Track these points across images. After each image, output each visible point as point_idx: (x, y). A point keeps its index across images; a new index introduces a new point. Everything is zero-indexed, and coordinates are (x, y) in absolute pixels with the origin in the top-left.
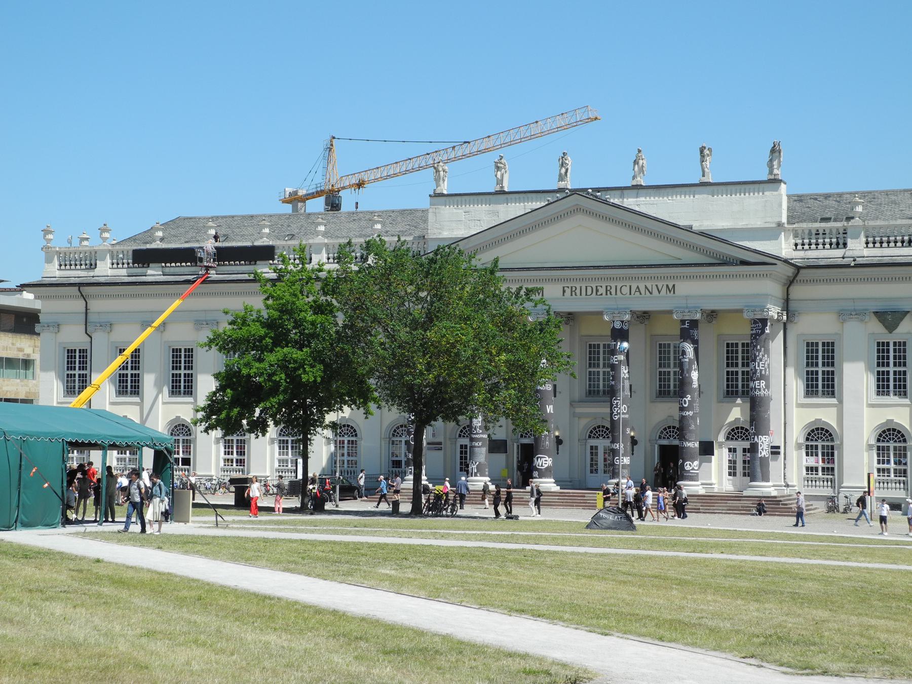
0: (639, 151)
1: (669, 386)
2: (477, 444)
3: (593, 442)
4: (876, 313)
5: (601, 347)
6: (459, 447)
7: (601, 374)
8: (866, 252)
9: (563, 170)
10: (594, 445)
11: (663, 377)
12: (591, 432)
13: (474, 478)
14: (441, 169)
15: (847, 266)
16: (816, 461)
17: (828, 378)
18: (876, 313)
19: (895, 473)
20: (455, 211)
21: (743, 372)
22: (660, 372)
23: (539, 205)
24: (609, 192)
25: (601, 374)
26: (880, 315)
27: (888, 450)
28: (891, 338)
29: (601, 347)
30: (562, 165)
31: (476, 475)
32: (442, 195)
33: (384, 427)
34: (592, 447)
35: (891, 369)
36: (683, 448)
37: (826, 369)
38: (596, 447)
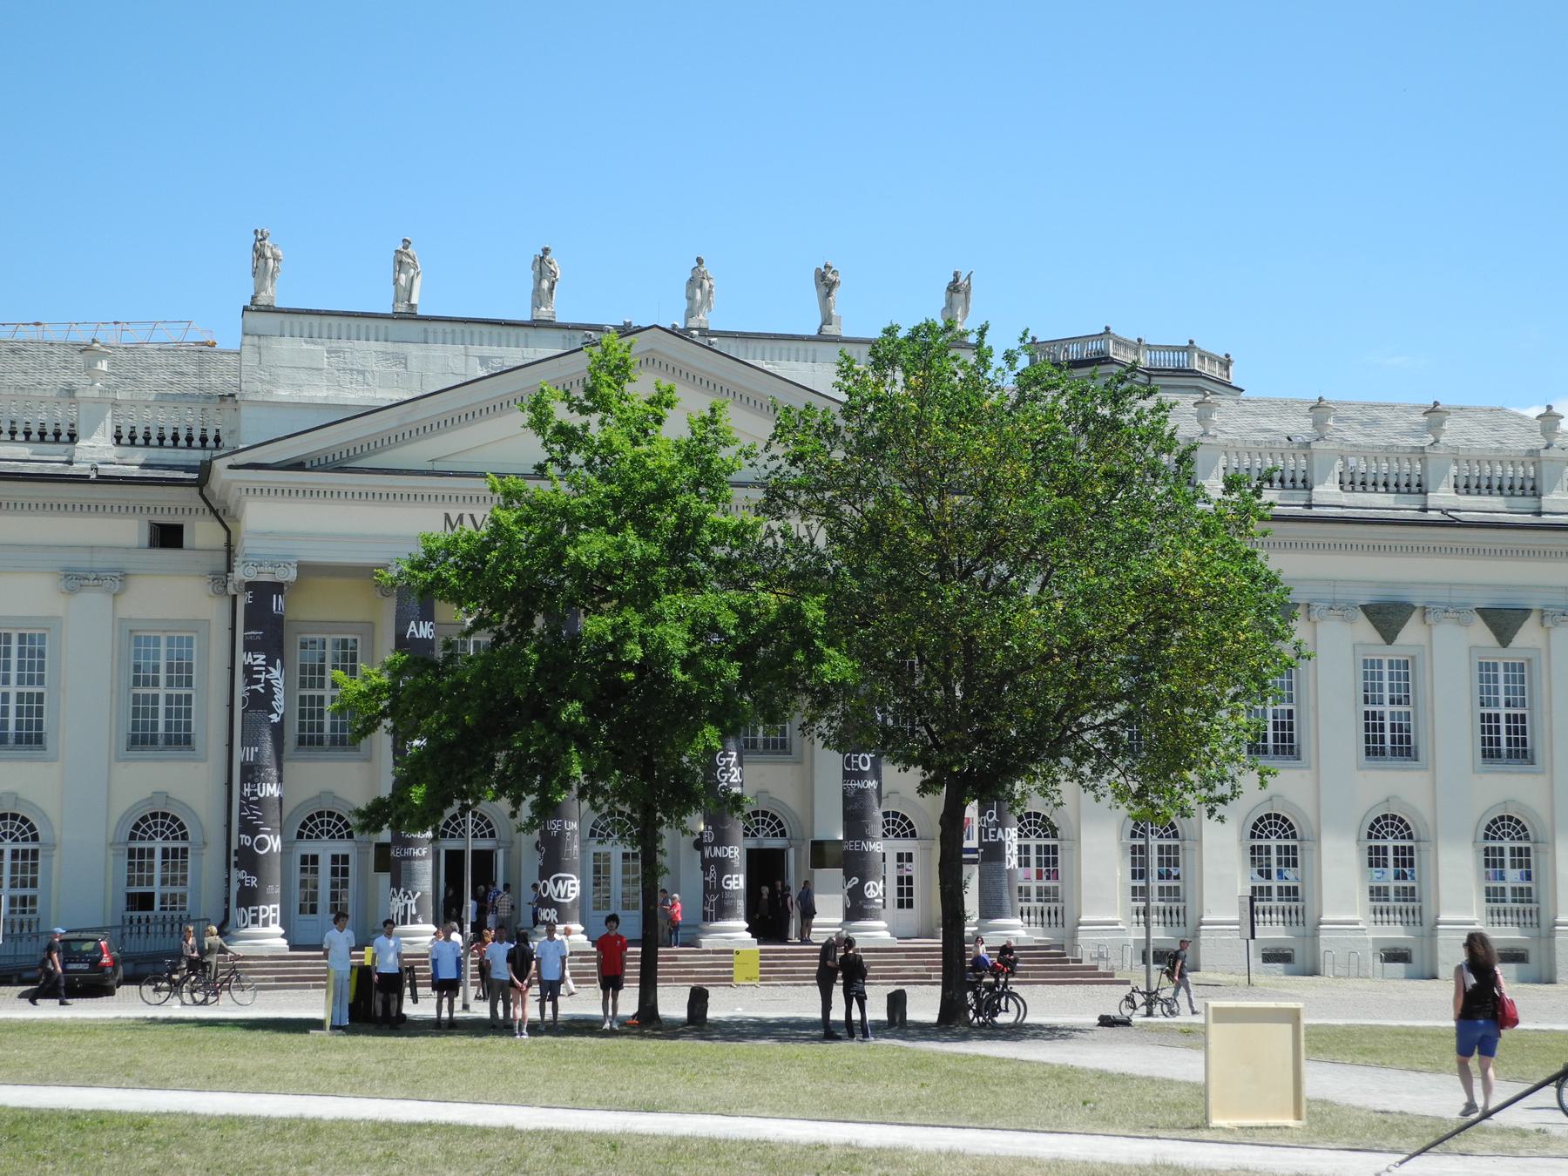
0: (700, 261)
1: (155, 725)
2: (417, 853)
3: (308, 847)
4: (1364, 608)
5: (163, 642)
6: (591, 856)
7: (162, 700)
8: (1346, 498)
9: (545, 284)
10: (310, 852)
11: (142, 709)
12: (137, 827)
13: (409, 927)
14: (269, 254)
15: (81, 479)
16: (1387, 878)
17: (178, 711)
18: (1364, 608)
19: (1280, 894)
20: (305, 346)
21: (1508, 716)
22: (302, 698)
23: (532, 354)
24: (752, 344)
25: (162, 700)
26: (1488, 615)
27: (1385, 853)
28: (1387, 653)
29: (163, 642)
30: (540, 276)
31: (414, 921)
32: (269, 310)
33: (114, 820)
34: (304, 859)
35: (162, 691)
36: (863, 854)
37: (175, 691)
38: (315, 859)
